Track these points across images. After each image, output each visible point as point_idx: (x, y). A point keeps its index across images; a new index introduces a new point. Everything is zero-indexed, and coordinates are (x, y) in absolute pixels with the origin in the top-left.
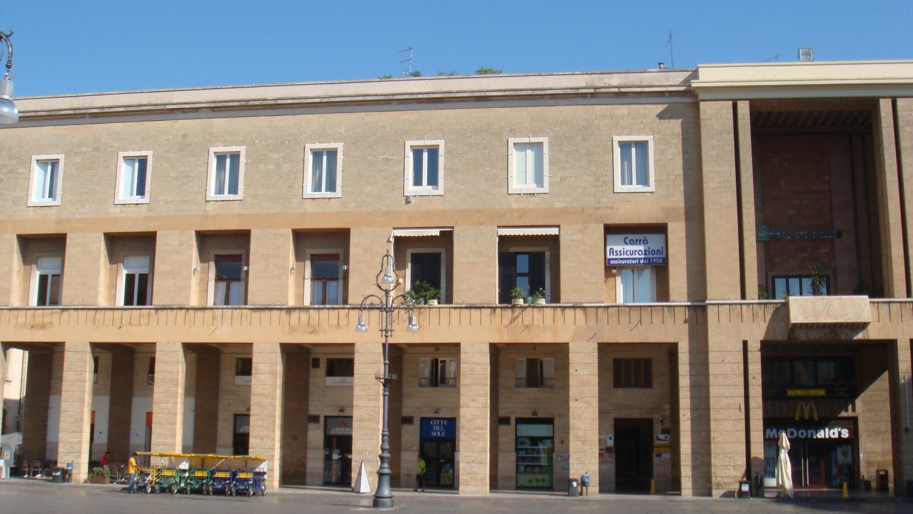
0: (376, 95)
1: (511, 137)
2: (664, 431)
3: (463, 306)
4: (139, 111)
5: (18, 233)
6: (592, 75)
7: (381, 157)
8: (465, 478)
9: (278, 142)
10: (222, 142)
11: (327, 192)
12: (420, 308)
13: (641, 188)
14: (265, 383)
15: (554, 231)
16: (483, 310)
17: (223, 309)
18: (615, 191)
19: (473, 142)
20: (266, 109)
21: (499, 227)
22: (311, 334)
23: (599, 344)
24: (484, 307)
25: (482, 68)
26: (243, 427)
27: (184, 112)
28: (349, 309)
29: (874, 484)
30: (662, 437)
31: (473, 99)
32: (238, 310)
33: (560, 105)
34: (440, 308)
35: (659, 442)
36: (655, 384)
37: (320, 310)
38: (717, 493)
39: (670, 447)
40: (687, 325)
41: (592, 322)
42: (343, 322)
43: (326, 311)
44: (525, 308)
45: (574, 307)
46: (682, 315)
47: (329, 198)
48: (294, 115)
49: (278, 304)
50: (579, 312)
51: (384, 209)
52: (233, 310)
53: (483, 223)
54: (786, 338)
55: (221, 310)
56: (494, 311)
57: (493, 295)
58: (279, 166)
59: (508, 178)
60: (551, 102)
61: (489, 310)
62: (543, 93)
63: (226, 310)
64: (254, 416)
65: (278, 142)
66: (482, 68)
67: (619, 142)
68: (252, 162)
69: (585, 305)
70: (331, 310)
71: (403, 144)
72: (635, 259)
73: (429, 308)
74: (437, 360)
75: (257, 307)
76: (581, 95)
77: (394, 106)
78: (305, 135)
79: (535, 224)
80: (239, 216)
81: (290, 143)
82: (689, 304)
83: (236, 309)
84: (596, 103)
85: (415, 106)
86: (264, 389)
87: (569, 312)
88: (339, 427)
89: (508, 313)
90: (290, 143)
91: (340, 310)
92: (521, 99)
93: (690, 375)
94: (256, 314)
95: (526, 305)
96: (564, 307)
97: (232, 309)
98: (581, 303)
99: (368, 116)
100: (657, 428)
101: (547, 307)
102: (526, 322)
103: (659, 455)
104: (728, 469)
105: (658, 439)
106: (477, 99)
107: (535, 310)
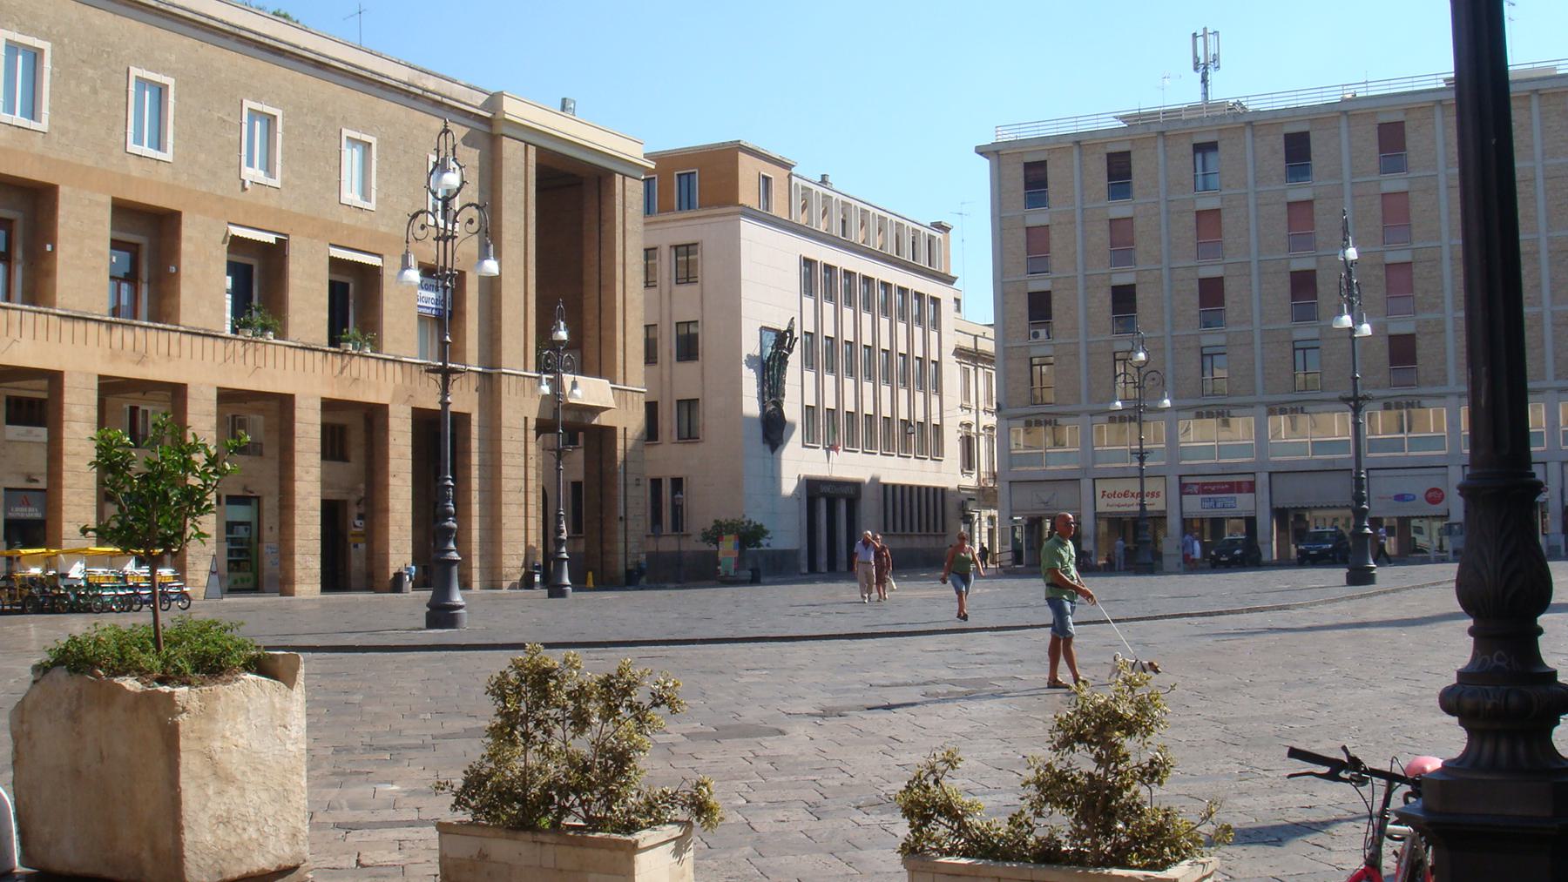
0: (221, 21)
1: (248, 99)
2: (360, 517)
3: (300, 345)
4: (298, 55)
5: (115, 196)
6: (414, 71)
7: (216, 115)
8: (300, 574)
9: (95, 51)
10: (17, 25)
11: (23, 118)
12: (256, 342)
13: (25, 122)
14: (81, 437)
15: (376, 261)
16: (317, 353)
17: (22, 310)
18: (128, 151)
19: (308, 123)
20: (249, 45)
21: (229, 223)
22: (137, 364)
23: (413, 408)
24: (317, 350)
25: (279, 10)
26: (12, 509)
27: (408, 97)
28: (181, 332)
29: (1136, 545)
30: (358, 523)
31: (313, 63)
32: (43, 315)
33: (387, 100)
34: (275, 344)
35: (354, 529)
36: (352, 459)
37: (148, 330)
38: (506, 584)
39: (363, 535)
40: (477, 394)
41: (408, 380)
42: (174, 350)
43: (154, 332)
44: (353, 355)
45: (393, 361)
46: (474, 381)
47: (158, 160)
48: (115, 13)
49: (96, 312)
50: (398, 366)
51: (219, 192)
52: (37, 314)
53: (316, 237)
54: (552, 418)
55: (19, 312)
56: (326, 355)
57: (321, 335)
58: (94, 91)
59: (340, 182)
60: (379, 92)
61: (321, 353)
62: (380, 79)
63: (27, 313)
64: (67, 488)
65: (95, 51)
66: (279, 10)
67: (7, 40)
68: (60, 72)
69: (404, 359)
70: (160, 332)
71: (240, 103)
72: (428, 308)
73: (265, 343)
74: (137, 408)
75: (70, 313)
76: (258, 45)
77: (231, 43)
78: (127, 51)
79: (372, 251)
80: (42, 158)
81: (109, 57)
82: (480, 369)
83: (40, 312)
84: (516, 137)
85: (252, 50)
86: (80, 446)
87: (390, 365)
88: (20, 506)
89: (338, 360)
90: (109, 57)
91: (171, 333)
92: (358, 81)
93: (480, 452)
94: (67, 326)
95: (355, 352)
96: (386, 360)
97: (35, 312)
98: (401, 357)
99: (202, 46)
100: (354, 511)
101: (372, 357)
102: (355, 374)
103: (356, 546)
104: (513, 559)
105: (355, 526)
106: (317, 64)
107: (362, 358)
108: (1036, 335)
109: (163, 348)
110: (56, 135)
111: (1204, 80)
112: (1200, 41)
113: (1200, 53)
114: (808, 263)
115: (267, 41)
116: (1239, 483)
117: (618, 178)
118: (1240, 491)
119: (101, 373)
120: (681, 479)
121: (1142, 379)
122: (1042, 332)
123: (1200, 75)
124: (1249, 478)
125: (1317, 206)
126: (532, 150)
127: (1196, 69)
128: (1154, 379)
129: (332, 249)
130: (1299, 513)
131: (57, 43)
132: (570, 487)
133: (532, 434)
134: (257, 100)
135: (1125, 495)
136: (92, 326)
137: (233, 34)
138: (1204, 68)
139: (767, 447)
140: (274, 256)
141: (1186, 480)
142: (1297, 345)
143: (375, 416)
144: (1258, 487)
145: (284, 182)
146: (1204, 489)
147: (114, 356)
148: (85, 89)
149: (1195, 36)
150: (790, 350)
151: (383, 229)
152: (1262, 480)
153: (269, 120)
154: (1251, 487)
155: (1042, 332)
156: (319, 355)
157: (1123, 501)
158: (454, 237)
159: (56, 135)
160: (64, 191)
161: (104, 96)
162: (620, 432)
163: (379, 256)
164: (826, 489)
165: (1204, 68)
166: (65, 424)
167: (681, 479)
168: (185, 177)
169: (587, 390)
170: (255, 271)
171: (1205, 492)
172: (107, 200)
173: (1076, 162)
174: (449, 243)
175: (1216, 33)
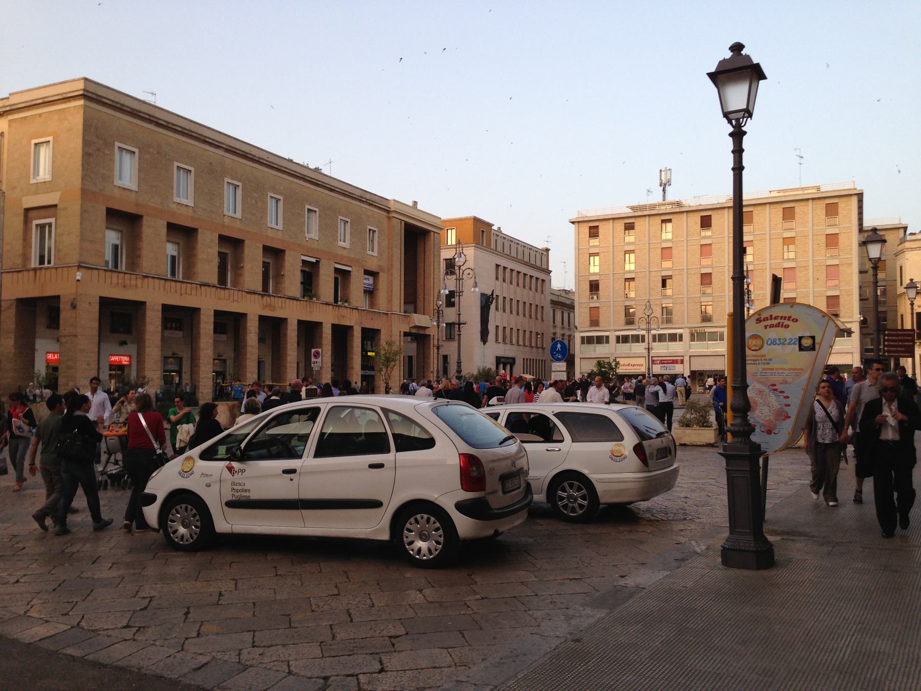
5: (169, 221)
7: (297, 211)
23: (362, 328)
50: (357, 311)
58: (256, 202)
87: (354, 310)
108: (592, 298)
109: (280, 305)
110: (244, 220)
111: (664, 190)
112: (663, 173)
113: (663, 178)
114: (498, 266)
115: (314, 181)
116: (677, 360)
117: (432, 233)
118: (677, 363)
119: (101, 295)
120: (447, 356)
121: (461, 273)
122: (595, 297)
123: (662, 188)
124: (681, 358)
125: (713, 246)
126: (403, 223)
127: (661, 186)
128: (469, 274)
129: (302, 256)
130: (54, 321)
131: (244, 184)
132: (407, 360)
133: (402, 337)
134: (310, 205)
135: (628, 365)
136: (256, 296)
137: (303, 178)
138: (664, 186)
139: (482, 343)
140: (315, 266)
141: (654, 359)
142: (703, 304)
143: (239, 318)
144: (685, 361)
145: (352, 243)
146: (662, 362)
147: (264, 307)
148: (253, 201)
149: (661, 171)
150: (492, 303)
151: (352, 256)
152: (686, 359)
153: (235, 188)
154: (682, 362)
155: (595, 297)
156: (331, 307)
157: (627, 367)
158: (463, 279)
159: (244, 220)
160: (247, 243)
161: (260, 204)
162: (432, 337)
163: (351, 266)
164: (503, 360)
165: (664, 186)
166: (248, 334)
167: (447, 356)
168: (287, 236)
169: (420, 320)
170: (271, 265)
171: (662, 364)
172: (261, 246)
173: (611, 227)
174: (461, 281)
175: (669, 170)
